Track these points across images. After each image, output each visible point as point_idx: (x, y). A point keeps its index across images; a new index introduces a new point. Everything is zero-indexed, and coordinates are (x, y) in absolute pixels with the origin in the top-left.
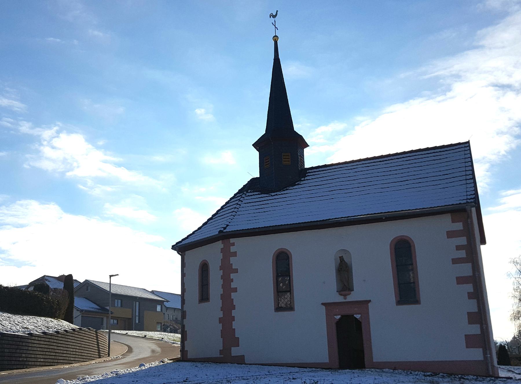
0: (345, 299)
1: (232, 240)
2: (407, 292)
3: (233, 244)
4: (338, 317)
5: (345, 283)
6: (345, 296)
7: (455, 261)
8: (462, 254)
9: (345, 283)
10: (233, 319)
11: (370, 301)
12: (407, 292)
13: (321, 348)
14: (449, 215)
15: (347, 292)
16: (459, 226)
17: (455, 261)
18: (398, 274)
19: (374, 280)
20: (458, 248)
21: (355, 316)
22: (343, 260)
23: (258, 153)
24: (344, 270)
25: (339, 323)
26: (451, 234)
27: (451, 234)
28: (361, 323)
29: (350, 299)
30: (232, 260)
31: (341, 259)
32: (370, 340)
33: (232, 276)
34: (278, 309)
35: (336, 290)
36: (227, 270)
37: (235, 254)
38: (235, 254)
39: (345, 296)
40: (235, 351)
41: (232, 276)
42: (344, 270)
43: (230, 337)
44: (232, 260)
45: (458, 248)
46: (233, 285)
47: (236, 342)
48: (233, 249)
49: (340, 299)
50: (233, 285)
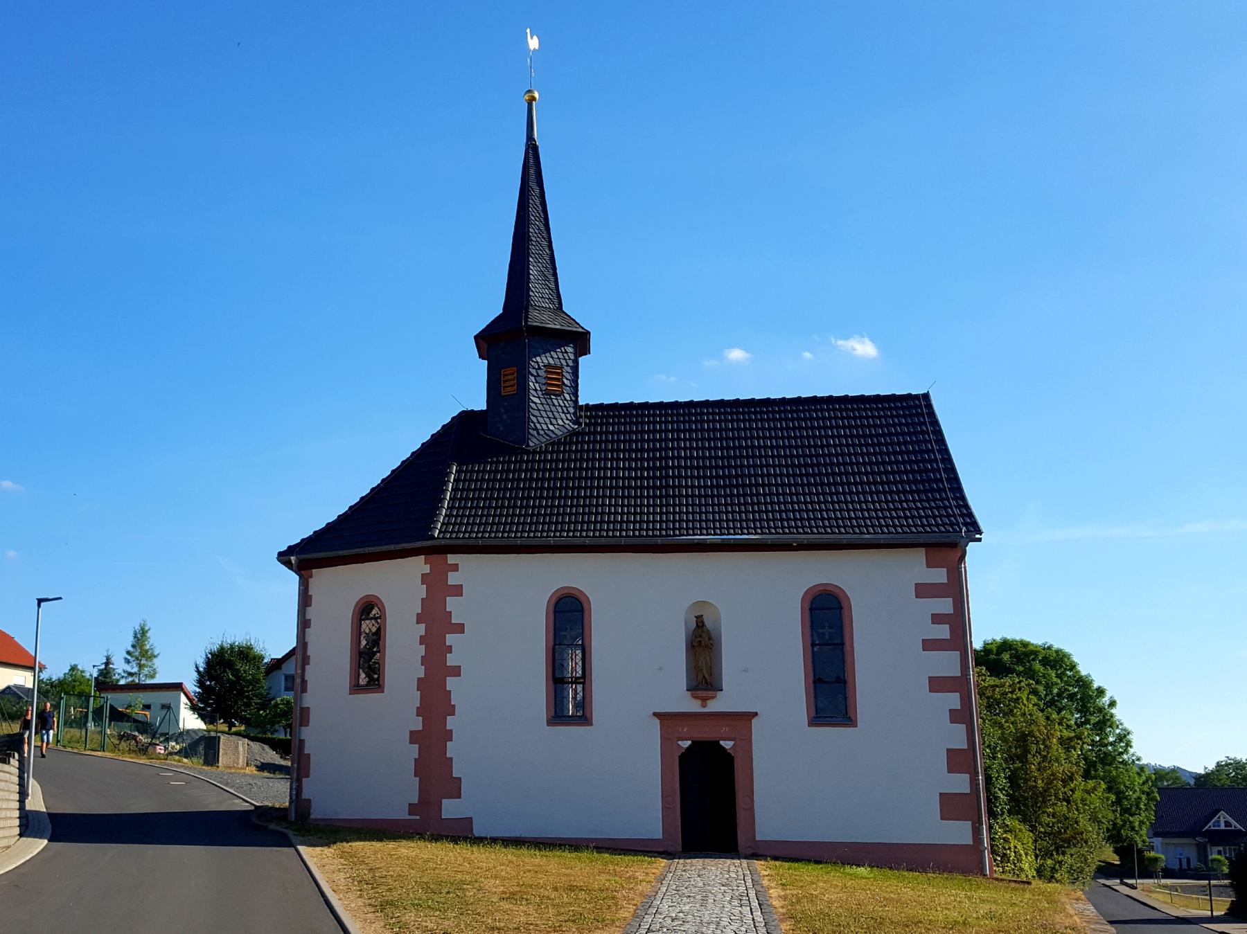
0: (704, 706)
1: (452, 559)
2: (831, 695)
3: (455, 568)
4: (686, 744)
5: (704, 679)
6: (704, 700)
7: (929, 645)
8: (943, 632)
9: (704, 679)
10: (449, 735)
11: (756, 714)
12: (831, 695)
13: (645, 800)
14: (923, 550)
15: (710, 693)
16: (939, 576)
17: (929, 645)
18: (816, 697)
19: (765, 674)
20: (937, 619)
21: (722, 743)
22: (703, 625)
23: (499, 311)
24: (702, 644)
25: (685, 757)
26: (923, 591)
27: (923, 591)
28: (732, 758)
29: (714, 706)
30: (452, 603)
31: (700, 622)
32: (751, 811)
33: (450, 639)
34: (558, 716)
35: (683, 684)
36: (437, 624)
37: (458, 591)
38: (458, 591)
39: (704, 700)
40: (450, 809)
41: (450, 639)
42: (702, 644)
43: (435, 774)
44: (452, 603)
45: (937, 619)
46: (451, 660)
47: (454, 788)
48: (453, 578)
49: (694, 706)
50: (451, 660)
